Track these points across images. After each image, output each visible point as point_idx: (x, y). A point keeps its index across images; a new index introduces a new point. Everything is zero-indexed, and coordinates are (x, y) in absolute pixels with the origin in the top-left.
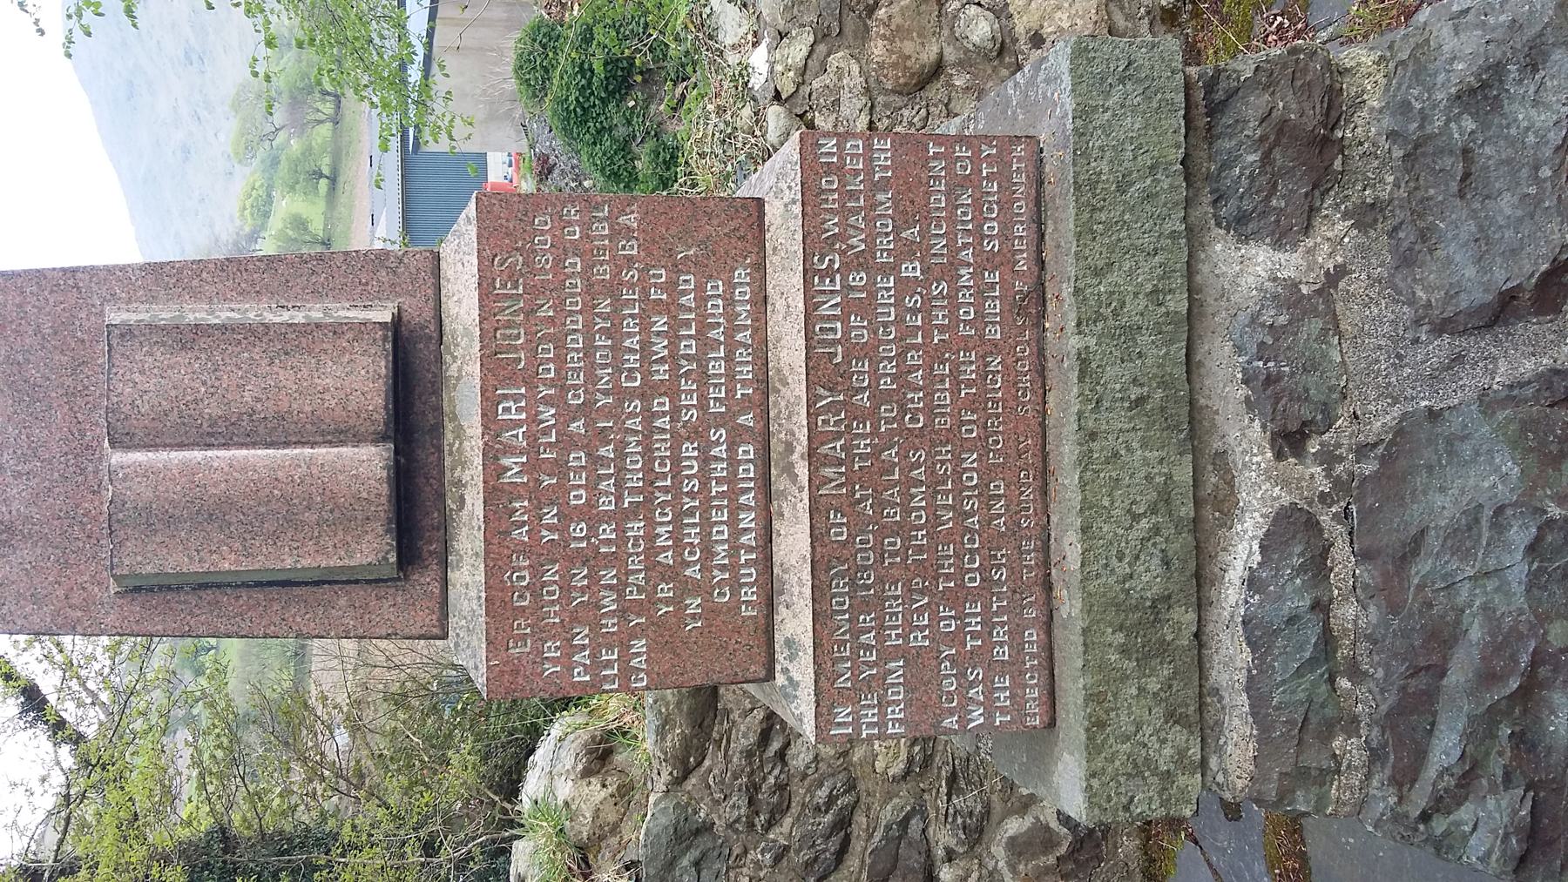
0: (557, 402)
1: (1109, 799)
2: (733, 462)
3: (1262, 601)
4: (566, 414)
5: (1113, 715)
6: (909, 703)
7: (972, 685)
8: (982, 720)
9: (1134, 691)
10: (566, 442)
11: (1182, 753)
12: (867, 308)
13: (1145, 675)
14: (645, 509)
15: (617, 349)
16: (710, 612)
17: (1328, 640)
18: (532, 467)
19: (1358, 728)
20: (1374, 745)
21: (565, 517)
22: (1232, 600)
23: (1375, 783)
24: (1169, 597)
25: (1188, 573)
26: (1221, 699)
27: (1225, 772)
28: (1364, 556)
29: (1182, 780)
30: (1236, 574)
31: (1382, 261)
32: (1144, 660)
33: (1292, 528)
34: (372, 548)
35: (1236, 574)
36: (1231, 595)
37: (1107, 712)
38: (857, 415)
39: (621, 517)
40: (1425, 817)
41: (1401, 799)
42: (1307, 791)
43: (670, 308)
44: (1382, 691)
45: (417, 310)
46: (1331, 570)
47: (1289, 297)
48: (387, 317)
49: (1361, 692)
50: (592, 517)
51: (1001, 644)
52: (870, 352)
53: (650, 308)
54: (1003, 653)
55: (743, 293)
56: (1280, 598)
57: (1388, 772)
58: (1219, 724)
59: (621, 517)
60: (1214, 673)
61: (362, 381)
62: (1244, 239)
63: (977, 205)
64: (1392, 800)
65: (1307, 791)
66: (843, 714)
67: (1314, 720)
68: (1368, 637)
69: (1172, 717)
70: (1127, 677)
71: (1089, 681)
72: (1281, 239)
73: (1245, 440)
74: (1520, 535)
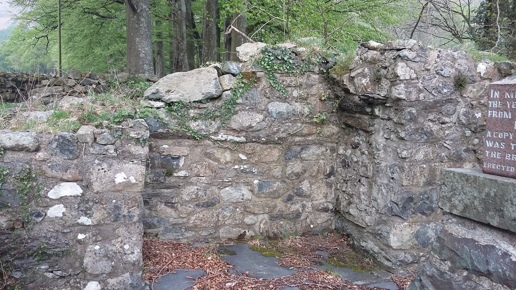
1: (447, 178)
3: (498, 255)
5: (469, 185)
6: (497, 119)
7: (499, 144)
8: (488, 146)
9: (475, 195)
11: (455, 207)
13: (480, 200)
17: (480, 274)
19: (451, 272)
20: (445, 275)
22: (502, 245)
23: (435, 270)
24: (503, 217)
25: (510, 227)
26: (472, 229)
27: (451, 223)
29: (448, 205)
32: (484, 201)
37: (471, 183)
40: (420, 280)
41: (427, 275)
42: (438, 247)
44: (458, 285)
46: (503, 286)
49: (460, 278)
51: (511, 157)
54: (508, 157)
56: (497, 261)
57: (436, 276)
58: (464, 226)
60: (481, 230)
64: (428, 273)
65: (438, 247)
66: (497, 95)
67: (457, 258)
68: (475, 287)
69: (466, 207)
70: (480, 194)
71: (481, 179)
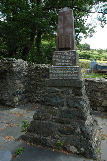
0: (66, 55)
2: (63, 64)
4: (65, 56)
10: (64, 56)
12: (70, 70)
15: (68, 58)
18: (63, 54)
21: (61, 56)
28: (56, 95)
30: (56, 89)
31: (71, 97)
33: (58, 92)
34: (60, 47)
35: (56, 89)
36: (55, 88)
43: (70, 61)
48: (71, 47)
50: (60, 57)
59: (60, 58)
61: (67, 46)
62: (73, 91)
63: (75, 76)
72: (72, 92)
73: (62, 90)
74: (56, 102)
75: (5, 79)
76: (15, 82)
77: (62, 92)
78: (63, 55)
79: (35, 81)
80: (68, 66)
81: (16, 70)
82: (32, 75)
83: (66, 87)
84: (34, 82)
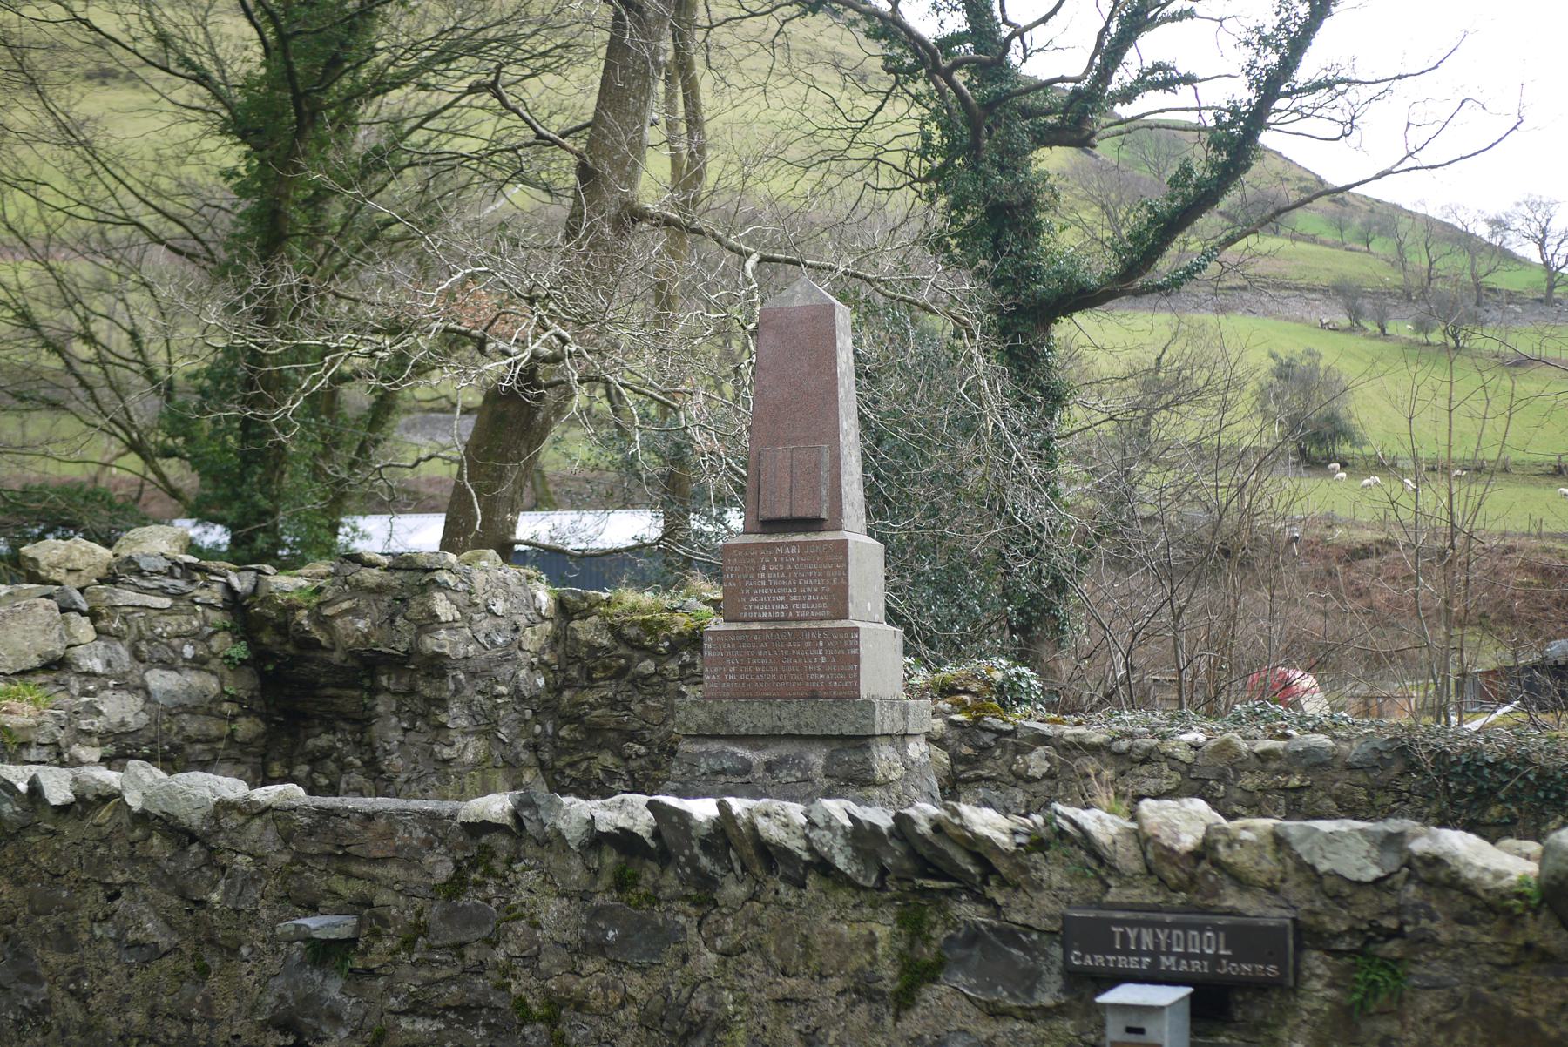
10: (785, 564)
14: (768, 585)
16: (742, 604)
18: (779, 555)
33: (747, 768)
34: (766, 514)
38: (785, 643)
39: (766, 579)
45: (826, 525)
47: (808, 767)
52: (802, 648)
53: (819, 587)
55: (823, 614)
75: (355, 721)
76: (447, 752)
77: (769, 767)
78: (779, 562)
79: (618, 753)
80: (804, 625)
81: (461, 652)
82: (591, 697)
83: (790, 737)
84: (608, 759)
